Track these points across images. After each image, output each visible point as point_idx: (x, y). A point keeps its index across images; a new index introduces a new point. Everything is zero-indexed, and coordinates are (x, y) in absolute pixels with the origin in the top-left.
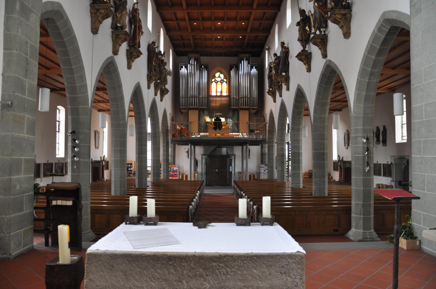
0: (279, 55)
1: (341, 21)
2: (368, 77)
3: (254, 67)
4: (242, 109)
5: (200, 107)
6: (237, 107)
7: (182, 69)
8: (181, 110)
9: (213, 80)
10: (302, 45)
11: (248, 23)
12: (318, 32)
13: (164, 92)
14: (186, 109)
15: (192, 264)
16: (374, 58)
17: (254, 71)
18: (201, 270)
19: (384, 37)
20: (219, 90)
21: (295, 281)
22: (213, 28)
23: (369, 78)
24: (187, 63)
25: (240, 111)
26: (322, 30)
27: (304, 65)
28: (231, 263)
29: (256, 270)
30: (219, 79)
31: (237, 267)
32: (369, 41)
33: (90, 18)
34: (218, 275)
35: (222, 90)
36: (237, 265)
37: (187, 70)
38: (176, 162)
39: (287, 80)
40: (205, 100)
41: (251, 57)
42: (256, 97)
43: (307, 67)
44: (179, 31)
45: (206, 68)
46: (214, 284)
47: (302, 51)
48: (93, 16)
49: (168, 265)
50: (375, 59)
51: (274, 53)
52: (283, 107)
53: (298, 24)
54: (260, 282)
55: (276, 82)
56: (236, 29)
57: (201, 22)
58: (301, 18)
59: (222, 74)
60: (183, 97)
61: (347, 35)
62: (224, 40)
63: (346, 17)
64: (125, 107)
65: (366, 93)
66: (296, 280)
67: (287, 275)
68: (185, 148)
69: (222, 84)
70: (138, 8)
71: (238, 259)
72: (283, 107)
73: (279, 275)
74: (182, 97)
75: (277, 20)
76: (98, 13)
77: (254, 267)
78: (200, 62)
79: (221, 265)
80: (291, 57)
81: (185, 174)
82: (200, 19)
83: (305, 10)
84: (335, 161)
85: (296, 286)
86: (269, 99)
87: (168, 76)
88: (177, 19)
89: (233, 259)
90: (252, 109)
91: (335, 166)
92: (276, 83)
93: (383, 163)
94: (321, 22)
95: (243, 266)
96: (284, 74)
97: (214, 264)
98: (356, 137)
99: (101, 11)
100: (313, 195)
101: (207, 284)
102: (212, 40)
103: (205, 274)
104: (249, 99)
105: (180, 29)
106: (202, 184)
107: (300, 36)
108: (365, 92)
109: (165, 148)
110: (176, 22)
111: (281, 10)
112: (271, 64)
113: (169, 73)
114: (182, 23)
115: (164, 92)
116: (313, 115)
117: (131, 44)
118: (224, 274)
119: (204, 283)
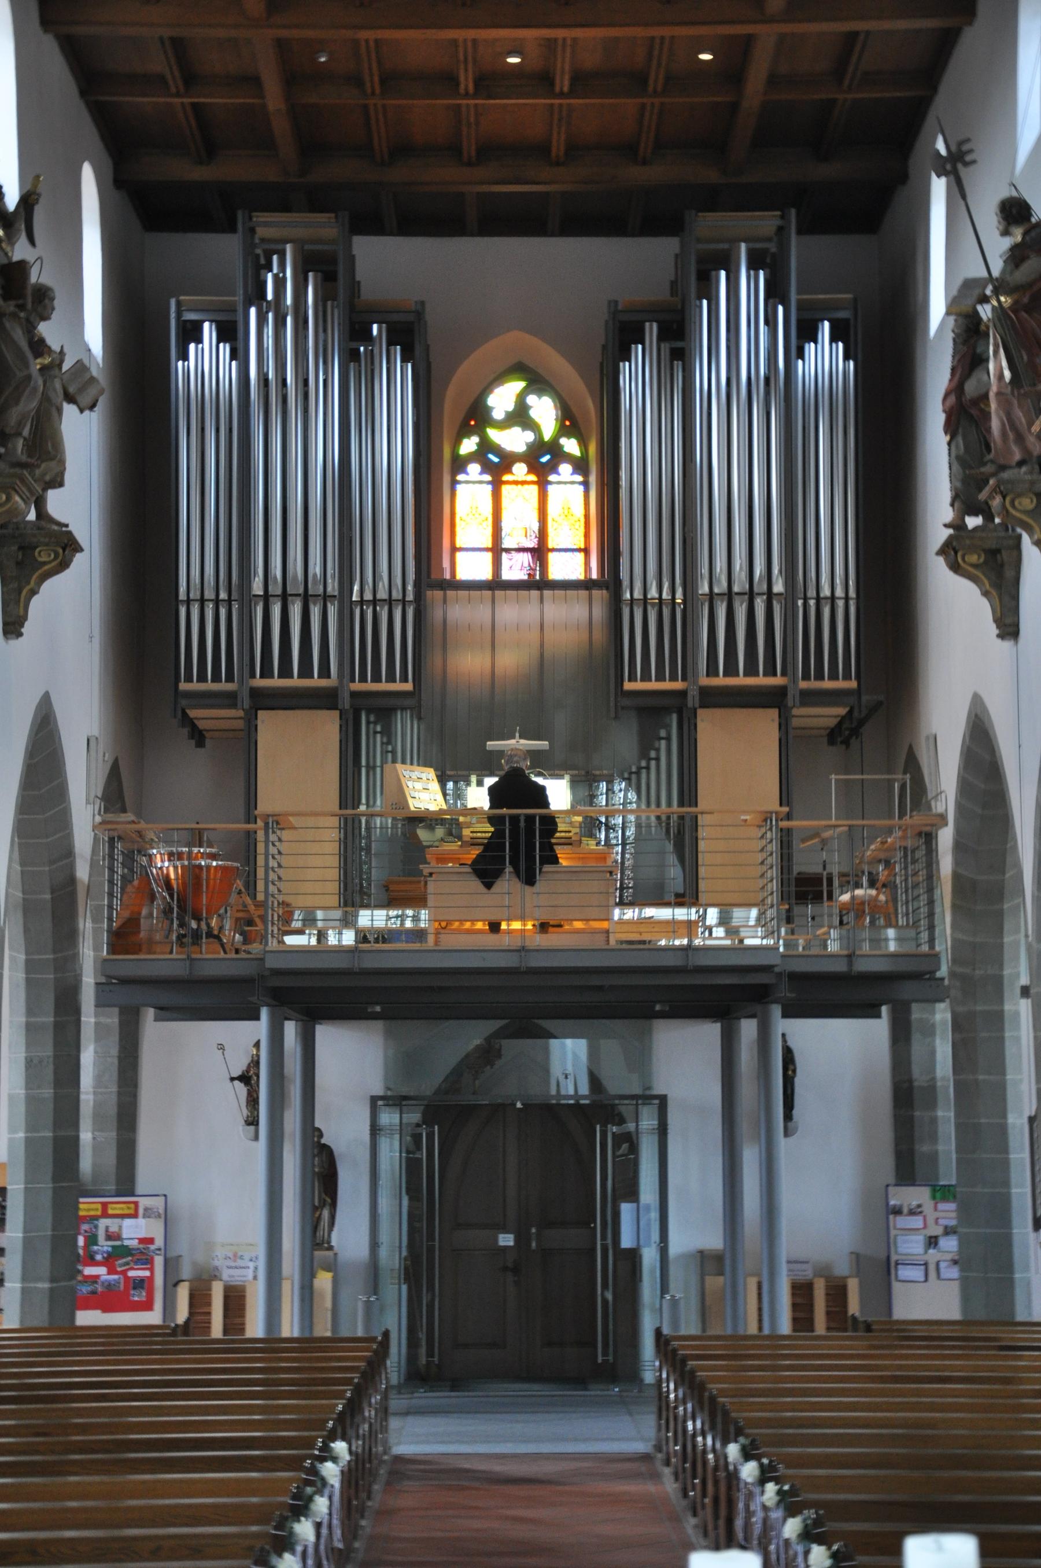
3: (827, 324)
5: (357, 686)
6: (673, 678)
8: (192, 713)
9: (469, 445)
14: (229, 699)
24: (239, 298)
25: (700, 712)
35: (542, 534)
37: (234, 356)
42: (839, 592)
55: (1017, 456)
60: (209, 594)
62: (564, 83)
68: (221, 1047)
69: (543, 485)
74: (195, 594)
78: (354, 287)
81: (226, 1275)
90: (810, 698)
92: (1021, 464)
110: (187, 100)
112: (977, 292)
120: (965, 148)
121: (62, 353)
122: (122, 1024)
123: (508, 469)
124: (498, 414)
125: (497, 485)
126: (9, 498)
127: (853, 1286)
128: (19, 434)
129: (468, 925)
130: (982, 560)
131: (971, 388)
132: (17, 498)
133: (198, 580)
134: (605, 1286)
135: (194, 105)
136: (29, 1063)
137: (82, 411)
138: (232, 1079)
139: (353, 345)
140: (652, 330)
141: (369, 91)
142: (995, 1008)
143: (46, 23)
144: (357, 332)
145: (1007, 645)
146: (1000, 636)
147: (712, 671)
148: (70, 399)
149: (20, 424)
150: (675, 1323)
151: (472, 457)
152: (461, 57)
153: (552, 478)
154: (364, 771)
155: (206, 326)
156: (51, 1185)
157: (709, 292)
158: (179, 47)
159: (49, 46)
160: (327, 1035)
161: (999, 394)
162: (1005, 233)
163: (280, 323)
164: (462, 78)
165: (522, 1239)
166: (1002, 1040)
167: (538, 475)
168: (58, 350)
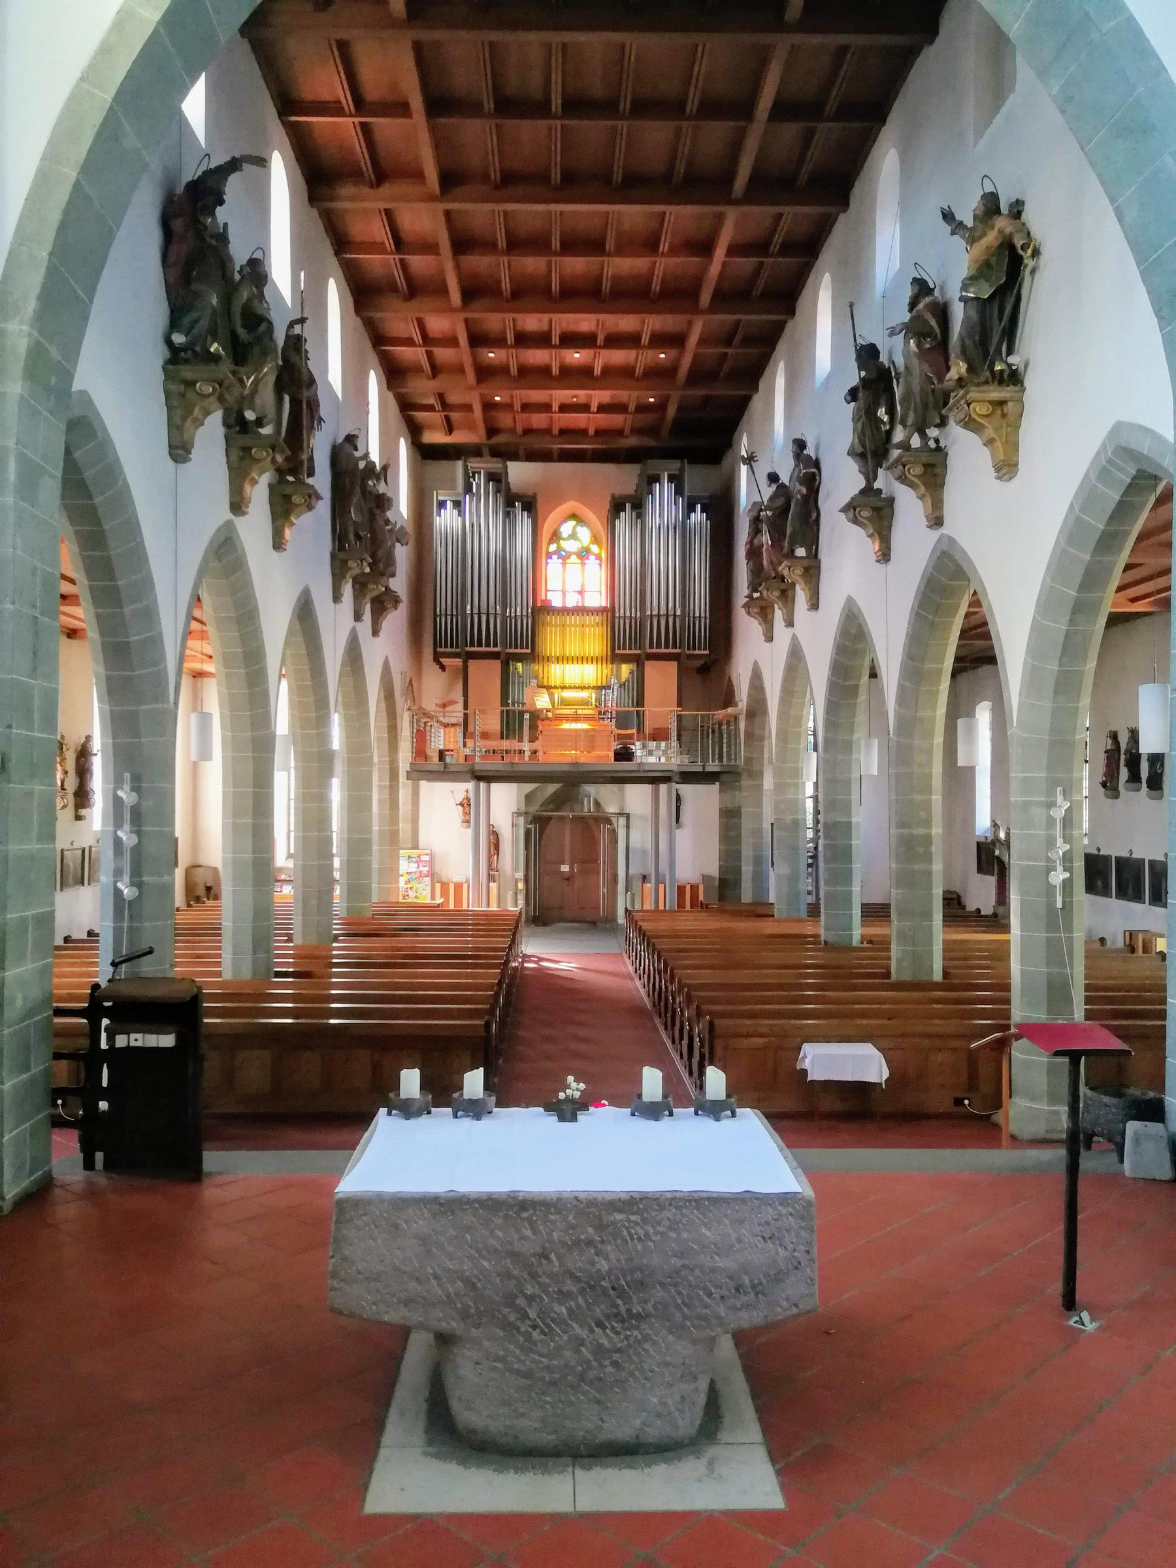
0: (785, 479)
1: (986, 424)
2: (1068, 618)
5: (509, 651)
6: (635, 649)
7: (443, 511)
8: (441, 660)
9: (553, 548)
10: (863, 470)
12: (916, 441)
13: (382, 604)
14: (457, 655)
15: (571, 1218)
16: (1088, 558)
18: (590, 1230)
19: (1118, 498)
20: (573, 585)
21: (793, 1257)
22: (555, 371)
23: (1070, 621)
25: (646, 663)
26: (933, 432)
27: (869, 539)
28: (654, 1214)
29: (709, 1229)
30: (570, 546)
31: (667, 1223)
32: (1072, 504)
33: (165, 409)
34: (627, 1241)
35: (583, 586)
36: (669, 1219)
38: (423, 839)
39: (811, 576)
42: (703, 615)
43: (877, 549)
44: (434, 378)
45: (529, 506)
46: (619, 1260)
47: (863, 492)
48: (175, 403)
49: (519, 1221)
50: (1089, 561)
51: (771, 470)
52: (796, 656)
53: (853, 394)
54: (716, 1258)
55: (773, 575)
56: (637, 374)
58: (863, 374)
60: (449, 612)
61: (1006, 468)
62: (594, 408)
63: (1005, 411)
65: (1061, 665)
66: (796, 1254)
67: (777, 1242)
68: (452, 792)
69: (583, 564)
70: (305, 335)
71: (670, 1205)
72: (796, 656)
73: (759, 1242)
75: (782, 347)
76: (190, 395)
77: (705, 1224)
78: (508, 489)
79: (633, 1218)
80: (828, 496)
81: (455, 880)
82: (510, 338)
83: (880, 348)
85: (796, 1268)
86: (747, 627)
89: (658, 1205)
90: (689, 657)
91: (983, 857)
92: (775, 578)
93: (1108, 899)
94: (925, 405)
95: (681, 1221)
96: (801, 552)
97: (619, 1217)
98: (1026, 806)
99: (200, 389)
101: (603, 1262)
102: (551, 407)
103: (598, 1239)
106: (518, 921)
107: (857, 440)
108: (1057, 662)
112: (758, 507)
113: (400, 537)
114: (443, 354)
115: (382, 604)
118: (640, 1239)
119: (597, 1259)
123: (569, 558)
124: (565, 535)
125: (564, 564)
131: (756, 541)
145: (768, 644)
147: (651, 646)
148: (398, 541)
150: (633, 904)
151: (555, 553)
153: (586, 561)
155: (448, 502)
157: (651, 492)
158: (441, 397)
162: (769, 486)
165: (572, 868)
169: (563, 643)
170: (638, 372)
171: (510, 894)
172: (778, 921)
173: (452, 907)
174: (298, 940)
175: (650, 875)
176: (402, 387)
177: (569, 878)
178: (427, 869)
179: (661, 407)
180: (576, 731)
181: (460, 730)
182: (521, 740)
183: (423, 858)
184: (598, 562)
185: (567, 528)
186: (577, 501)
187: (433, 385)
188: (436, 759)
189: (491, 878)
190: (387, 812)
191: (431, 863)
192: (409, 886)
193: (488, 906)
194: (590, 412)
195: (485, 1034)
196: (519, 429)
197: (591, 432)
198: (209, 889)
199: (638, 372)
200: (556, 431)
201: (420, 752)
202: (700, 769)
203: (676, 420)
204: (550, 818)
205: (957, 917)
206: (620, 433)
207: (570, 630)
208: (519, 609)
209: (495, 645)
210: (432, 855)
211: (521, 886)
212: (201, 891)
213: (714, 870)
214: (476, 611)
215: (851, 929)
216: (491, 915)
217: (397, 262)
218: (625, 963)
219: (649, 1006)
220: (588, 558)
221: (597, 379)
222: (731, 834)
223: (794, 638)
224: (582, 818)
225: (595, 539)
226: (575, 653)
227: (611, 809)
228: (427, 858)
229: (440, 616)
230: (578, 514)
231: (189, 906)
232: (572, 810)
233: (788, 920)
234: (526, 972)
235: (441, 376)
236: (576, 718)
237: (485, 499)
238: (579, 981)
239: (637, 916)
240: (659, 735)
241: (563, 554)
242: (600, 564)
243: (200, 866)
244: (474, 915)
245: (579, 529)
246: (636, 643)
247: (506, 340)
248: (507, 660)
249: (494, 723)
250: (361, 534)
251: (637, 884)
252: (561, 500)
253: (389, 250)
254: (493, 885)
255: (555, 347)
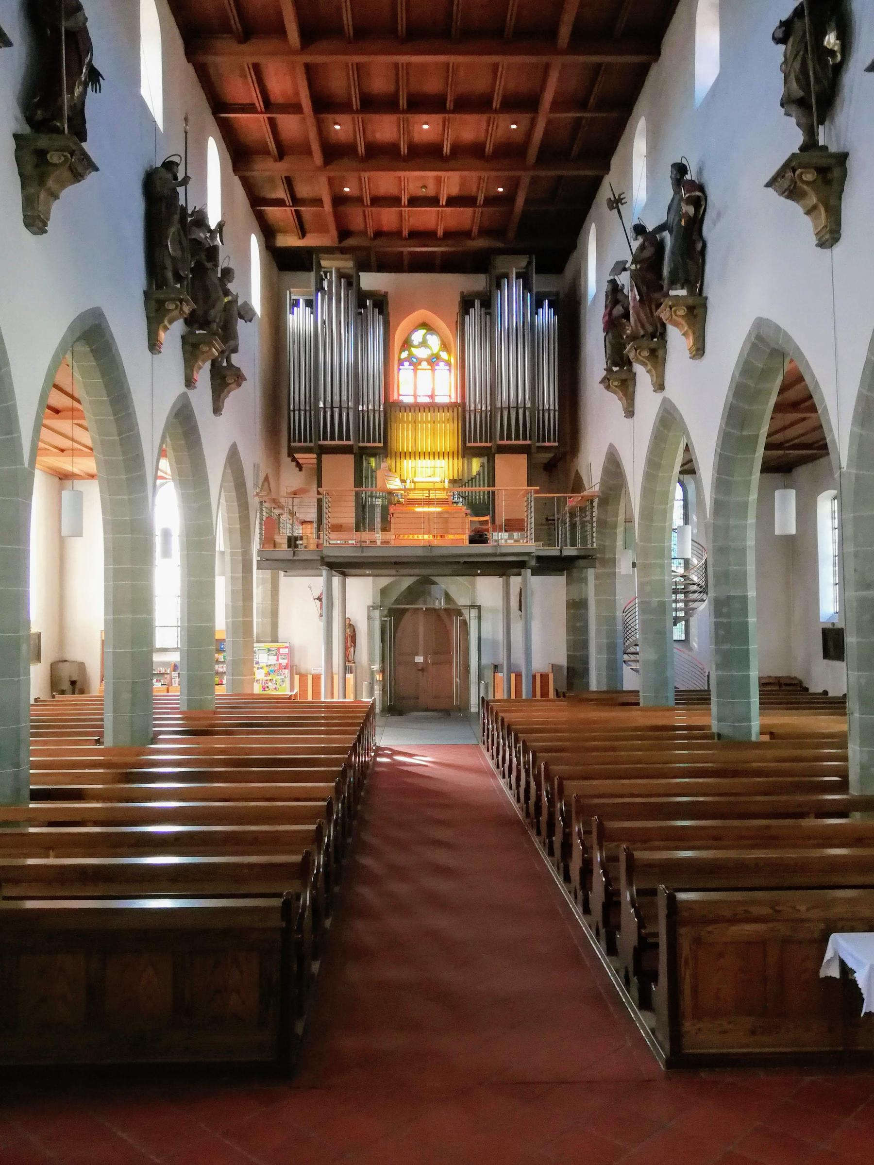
3: (547, 301)
4: (502, 449)
5: (361, 444)
6: (486, 441)
7: (295, 309)
8: (297, 456)
9: (404, 355)
11: (533, 123)
17: (546, 317)
24: (313, 289)
25: (497, 455)
30: (421, 353)
37: (312, 313)
38: (282, 633)
39: (695, 316)
40: (379, 419)
41: (536, 273)
42: (552, 408)
47: (803, 149)
57: (360, 116)
59: (431, 334)
60: (302, 408)
62: (443, 201)
64: (13, 398)
68: (310, 587)
69: (433, 370)
74: (297, 408)
81: (313, 672)
82: (356, 103)
84: (831, 626)
87: (240, 322)
88: (269, 105)
92: (643, 336)
100: (855, 791)
104: (527, 413)
105: (282, 152)
109: (239, 587)
110: (293, 209)
111: (663, 52)
112: (622, 266)
114: (290, 125)
116: (852, 434)
117: (39, 114)
120: (622, 197)
121: (237, 296)
122: (272, 578)
123: (420, 364)
124: (416, 343)
126: (210, 349)
127: (551, 677)
128: (214, 321)
129: (406, 537)
130: (619, 384)
132: (214, 350)
133: (298, 402)
134: (457, 677)
135: (296, 211)
136: (233, 591)
137: (246, 322)
138: (314, 599)
139: (360, 310)
140: (477, 303)
141: (366, 204)
142: (612, 570)
143: (236, 169)
144: (361, 304)
146: (655, 391)
147: (502, 438)
148: (242, 317)
149: (215, 317)
151: (406, 360)
152: (403, 187)
153: (436, 367)
154: (364, 479)
156: (749, 620)
159: (237, 181)
160: (350, 581)
161: (634, 307)
163: (330, 300)
164: (403, 198)
165: (426, 660)
166: (615, 583)
167: (431, 366)
168: (235, 294)
169: (415, 439)
170: (489, 149)
171: (365, 684)
172: (645, 710)
173: (310, 698)
174: (108, 741)
175: (502, 665)
176: (247, 170)
177: (422, 669)
178: (286, 661)
179: (509, 199)
180: (429, 513)
181: (315, 525)
182: (372, 529)
183: (282, 651)
184: (447, 368)
185: (417, 336)
186: (425, 309)
187: (280, 168)
188: (285, 546)
189: (347, 669)
190: (240, 603)
191: (290, 655)
192: (270, 678)
193: (345, 697)
194: (440, 207)
195: (284, 924)
196: (370, 232)
197: (440, 233)
198: (73, 683)
199: (489, 149)
200: (405, 233)
201: (268, 540)
202: (557, 553)
203: (525, 214)
204: (405, 611)
205: (792, 703)
206: (467, 234)
207: (422, 427)
208: (371, 404)
209: (348, 439)
210: (290, 648)
211: (378, 677)
212: (66, 686)
213: (562, 660)
214: (328, 405)
215: (749, 720)
216: (334, 707)
217: (266, 119)
218: (483, 756)
219: (521, 815)
220: (438, 365)
221: (440, 239)
222: (578, 624)
223: (666, 401)
224: (435, 610)
225: (445, 346)
226: (427, 448)
227: (462, 601)
228: (286, 651)
229: (294, 411)
230: (427, 322)
231: (53, 697)
232: (425, 603)
233: (655, 709)
234: (378, 769)
235: (286, 158)
236: (429, 502)
237: (336, 304)
238: (437, 779)
239: (496, 706)
240: (512, 526)
241: (415, 360)
242: (450, 370)
243: (66, 661)
244: (327, 707)
245: (429, 337)
246: (486, 436)
247: (352, 105)
248: (361, 455)
249: (347, 515)
250: (182, 274)
251: (488, 673)
252: (412, 309)
253: (288, 204)
254: (350, 677)
255: (404, 112)
